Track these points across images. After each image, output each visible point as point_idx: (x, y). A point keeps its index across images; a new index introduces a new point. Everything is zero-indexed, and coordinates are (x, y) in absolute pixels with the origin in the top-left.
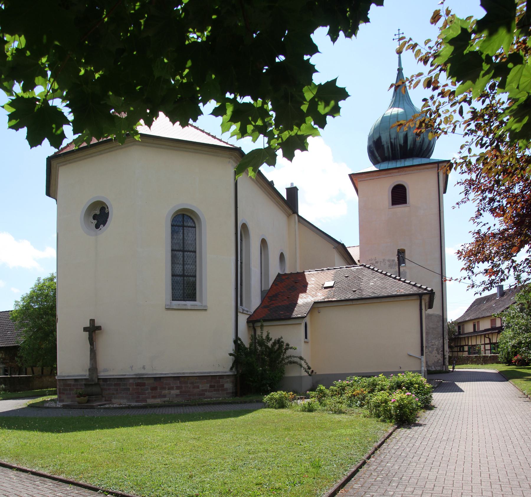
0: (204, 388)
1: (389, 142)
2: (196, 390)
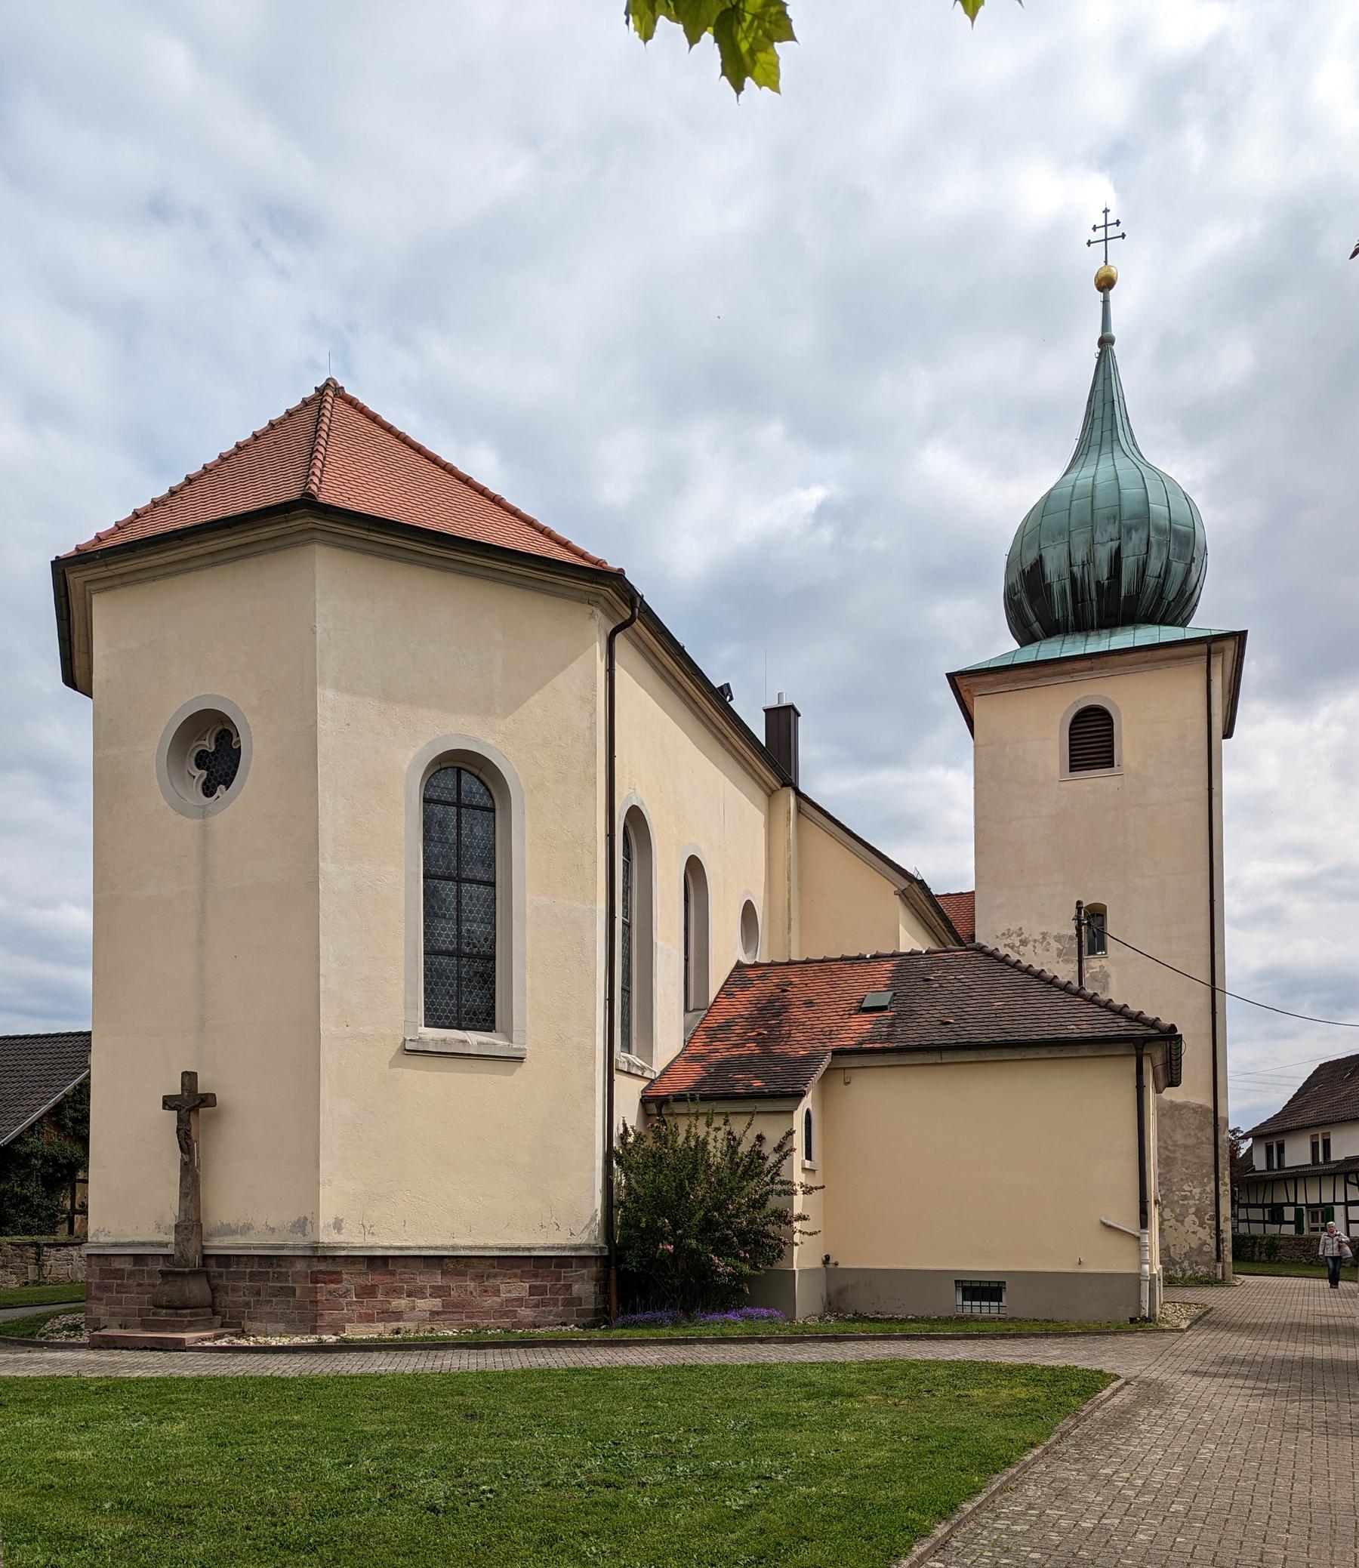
0: (514, 1295)
1: (1067, 575)
2: (491, 1301)
